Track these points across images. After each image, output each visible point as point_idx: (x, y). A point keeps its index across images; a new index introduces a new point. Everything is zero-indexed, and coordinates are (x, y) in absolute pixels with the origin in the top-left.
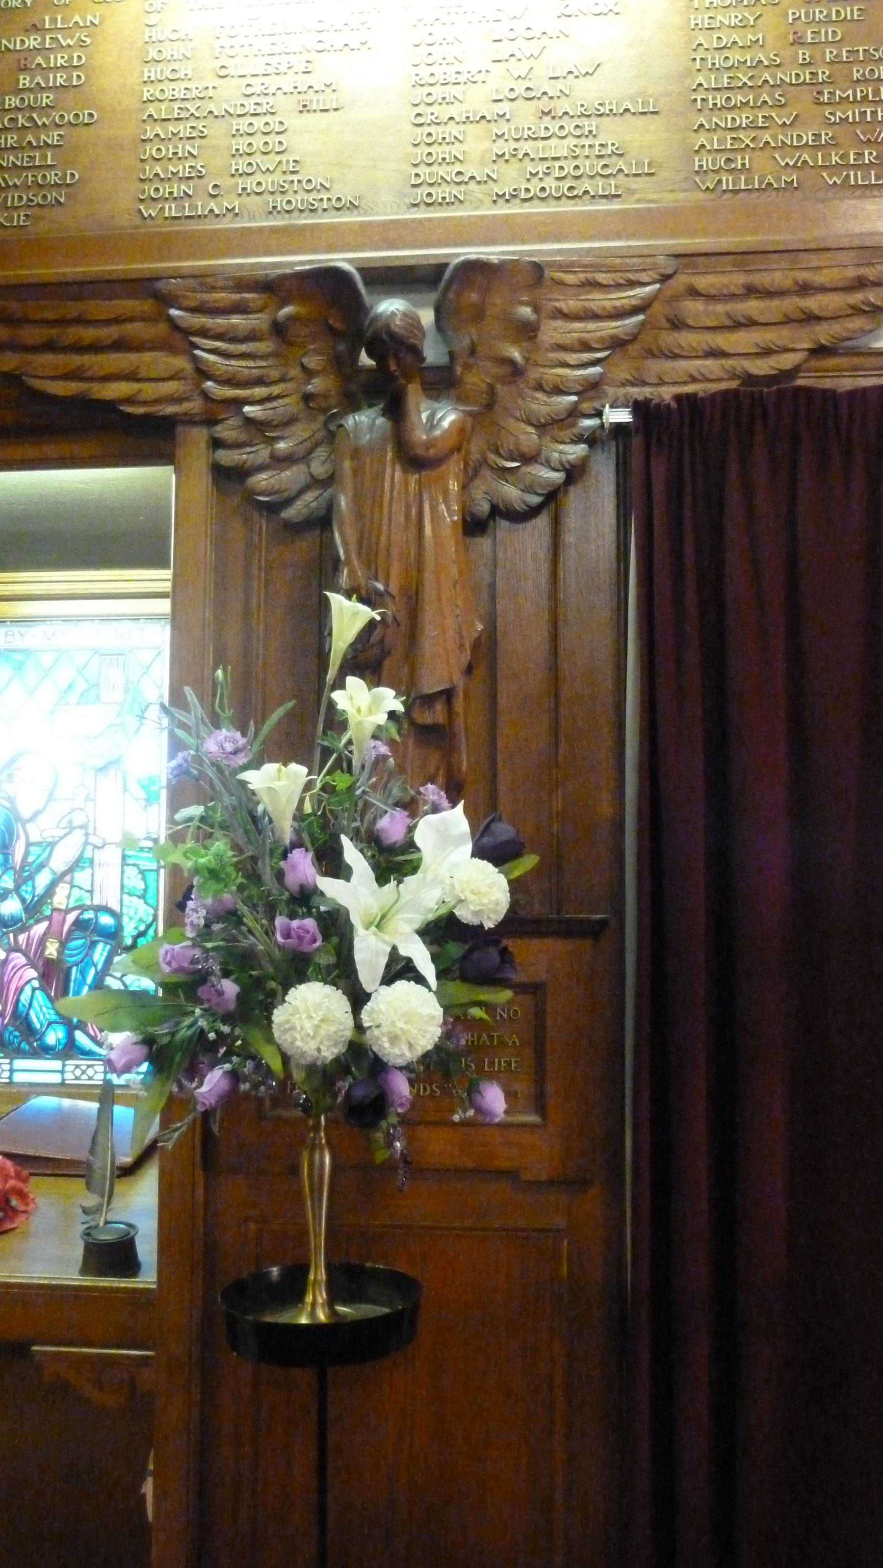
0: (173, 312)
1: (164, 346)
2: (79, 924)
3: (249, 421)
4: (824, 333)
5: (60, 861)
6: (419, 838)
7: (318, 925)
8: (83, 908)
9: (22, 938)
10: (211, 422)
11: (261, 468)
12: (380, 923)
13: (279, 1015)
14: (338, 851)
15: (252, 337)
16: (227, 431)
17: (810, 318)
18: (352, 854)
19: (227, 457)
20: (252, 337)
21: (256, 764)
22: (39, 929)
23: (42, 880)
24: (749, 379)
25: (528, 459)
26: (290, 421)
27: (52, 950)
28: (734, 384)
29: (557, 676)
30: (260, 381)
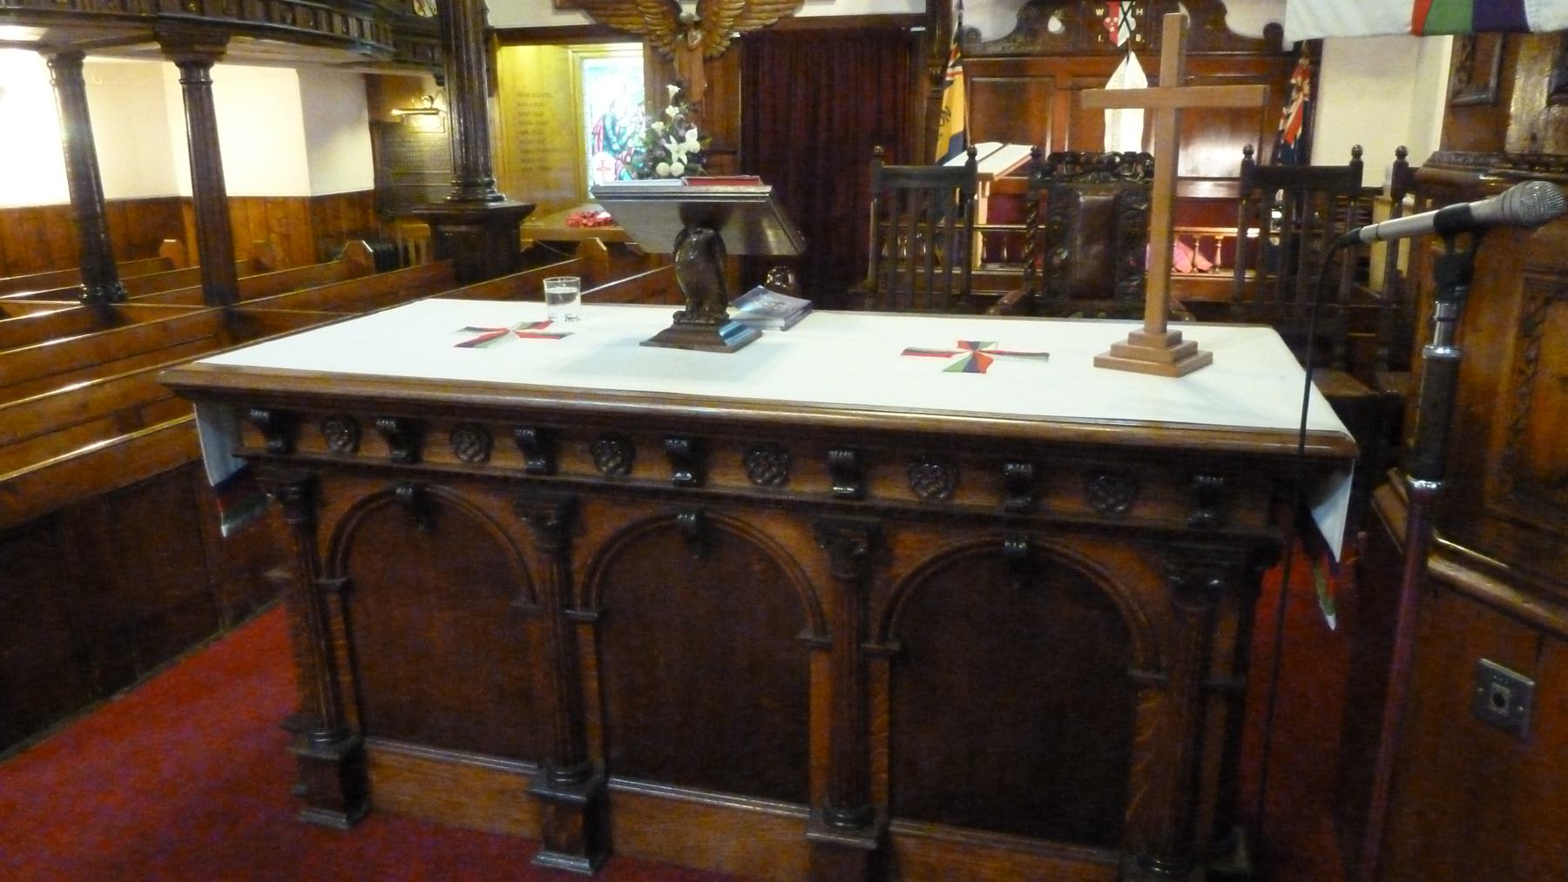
0: (640, 8)
1: (637, 16)
2: (636, 152)
3: (658, 36)
4: (781, 14)
5: (629, 132)
6: (686, 136)
7: (1392, 186)
8: (637, 147)
9: (620, 156)
10: (650, 35)
11: (661, 47)
12: (678, 152)
13: (657, 168)
14: (669, 138)
15: (657, 14)
16: (653, 37)
17: (778, 10)
18: (672, 138)
19: (654, 44)
20: (657, 14)
21: (653, 122)
22: (625, 153)
23: (624, 139)
24: (766, 26)
25: (718, 45)
26: (667, 35)
27: (628, 159)
28: (760, 27)
29: (56, 374)
30: (659, 25)
